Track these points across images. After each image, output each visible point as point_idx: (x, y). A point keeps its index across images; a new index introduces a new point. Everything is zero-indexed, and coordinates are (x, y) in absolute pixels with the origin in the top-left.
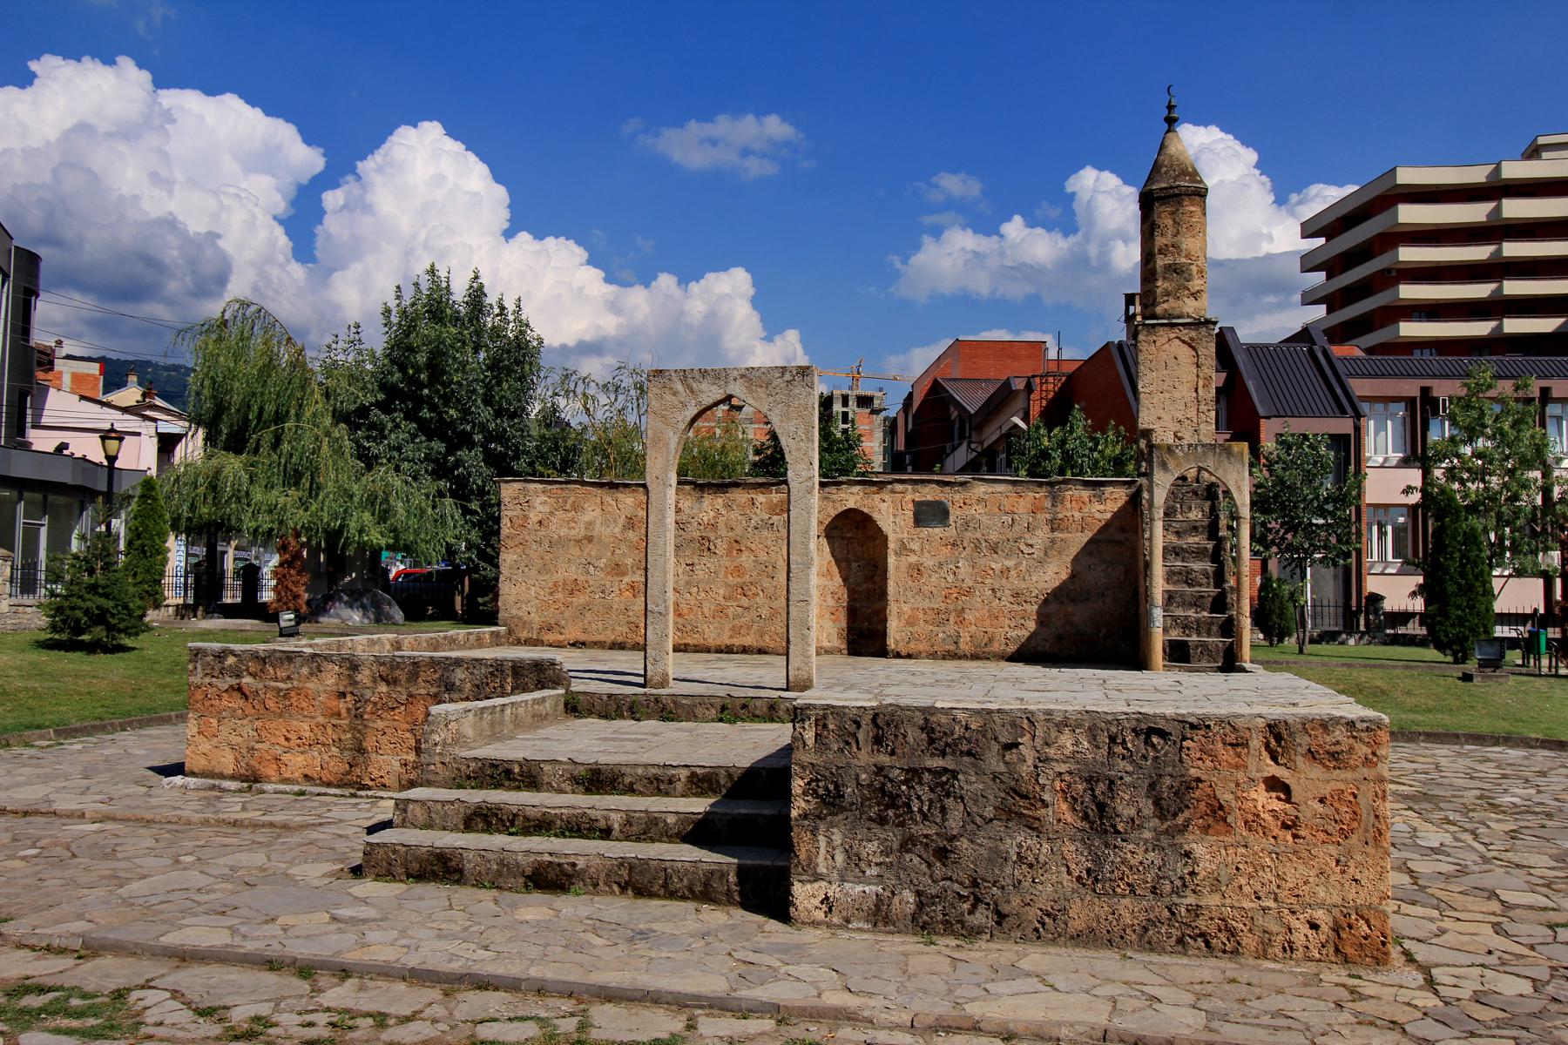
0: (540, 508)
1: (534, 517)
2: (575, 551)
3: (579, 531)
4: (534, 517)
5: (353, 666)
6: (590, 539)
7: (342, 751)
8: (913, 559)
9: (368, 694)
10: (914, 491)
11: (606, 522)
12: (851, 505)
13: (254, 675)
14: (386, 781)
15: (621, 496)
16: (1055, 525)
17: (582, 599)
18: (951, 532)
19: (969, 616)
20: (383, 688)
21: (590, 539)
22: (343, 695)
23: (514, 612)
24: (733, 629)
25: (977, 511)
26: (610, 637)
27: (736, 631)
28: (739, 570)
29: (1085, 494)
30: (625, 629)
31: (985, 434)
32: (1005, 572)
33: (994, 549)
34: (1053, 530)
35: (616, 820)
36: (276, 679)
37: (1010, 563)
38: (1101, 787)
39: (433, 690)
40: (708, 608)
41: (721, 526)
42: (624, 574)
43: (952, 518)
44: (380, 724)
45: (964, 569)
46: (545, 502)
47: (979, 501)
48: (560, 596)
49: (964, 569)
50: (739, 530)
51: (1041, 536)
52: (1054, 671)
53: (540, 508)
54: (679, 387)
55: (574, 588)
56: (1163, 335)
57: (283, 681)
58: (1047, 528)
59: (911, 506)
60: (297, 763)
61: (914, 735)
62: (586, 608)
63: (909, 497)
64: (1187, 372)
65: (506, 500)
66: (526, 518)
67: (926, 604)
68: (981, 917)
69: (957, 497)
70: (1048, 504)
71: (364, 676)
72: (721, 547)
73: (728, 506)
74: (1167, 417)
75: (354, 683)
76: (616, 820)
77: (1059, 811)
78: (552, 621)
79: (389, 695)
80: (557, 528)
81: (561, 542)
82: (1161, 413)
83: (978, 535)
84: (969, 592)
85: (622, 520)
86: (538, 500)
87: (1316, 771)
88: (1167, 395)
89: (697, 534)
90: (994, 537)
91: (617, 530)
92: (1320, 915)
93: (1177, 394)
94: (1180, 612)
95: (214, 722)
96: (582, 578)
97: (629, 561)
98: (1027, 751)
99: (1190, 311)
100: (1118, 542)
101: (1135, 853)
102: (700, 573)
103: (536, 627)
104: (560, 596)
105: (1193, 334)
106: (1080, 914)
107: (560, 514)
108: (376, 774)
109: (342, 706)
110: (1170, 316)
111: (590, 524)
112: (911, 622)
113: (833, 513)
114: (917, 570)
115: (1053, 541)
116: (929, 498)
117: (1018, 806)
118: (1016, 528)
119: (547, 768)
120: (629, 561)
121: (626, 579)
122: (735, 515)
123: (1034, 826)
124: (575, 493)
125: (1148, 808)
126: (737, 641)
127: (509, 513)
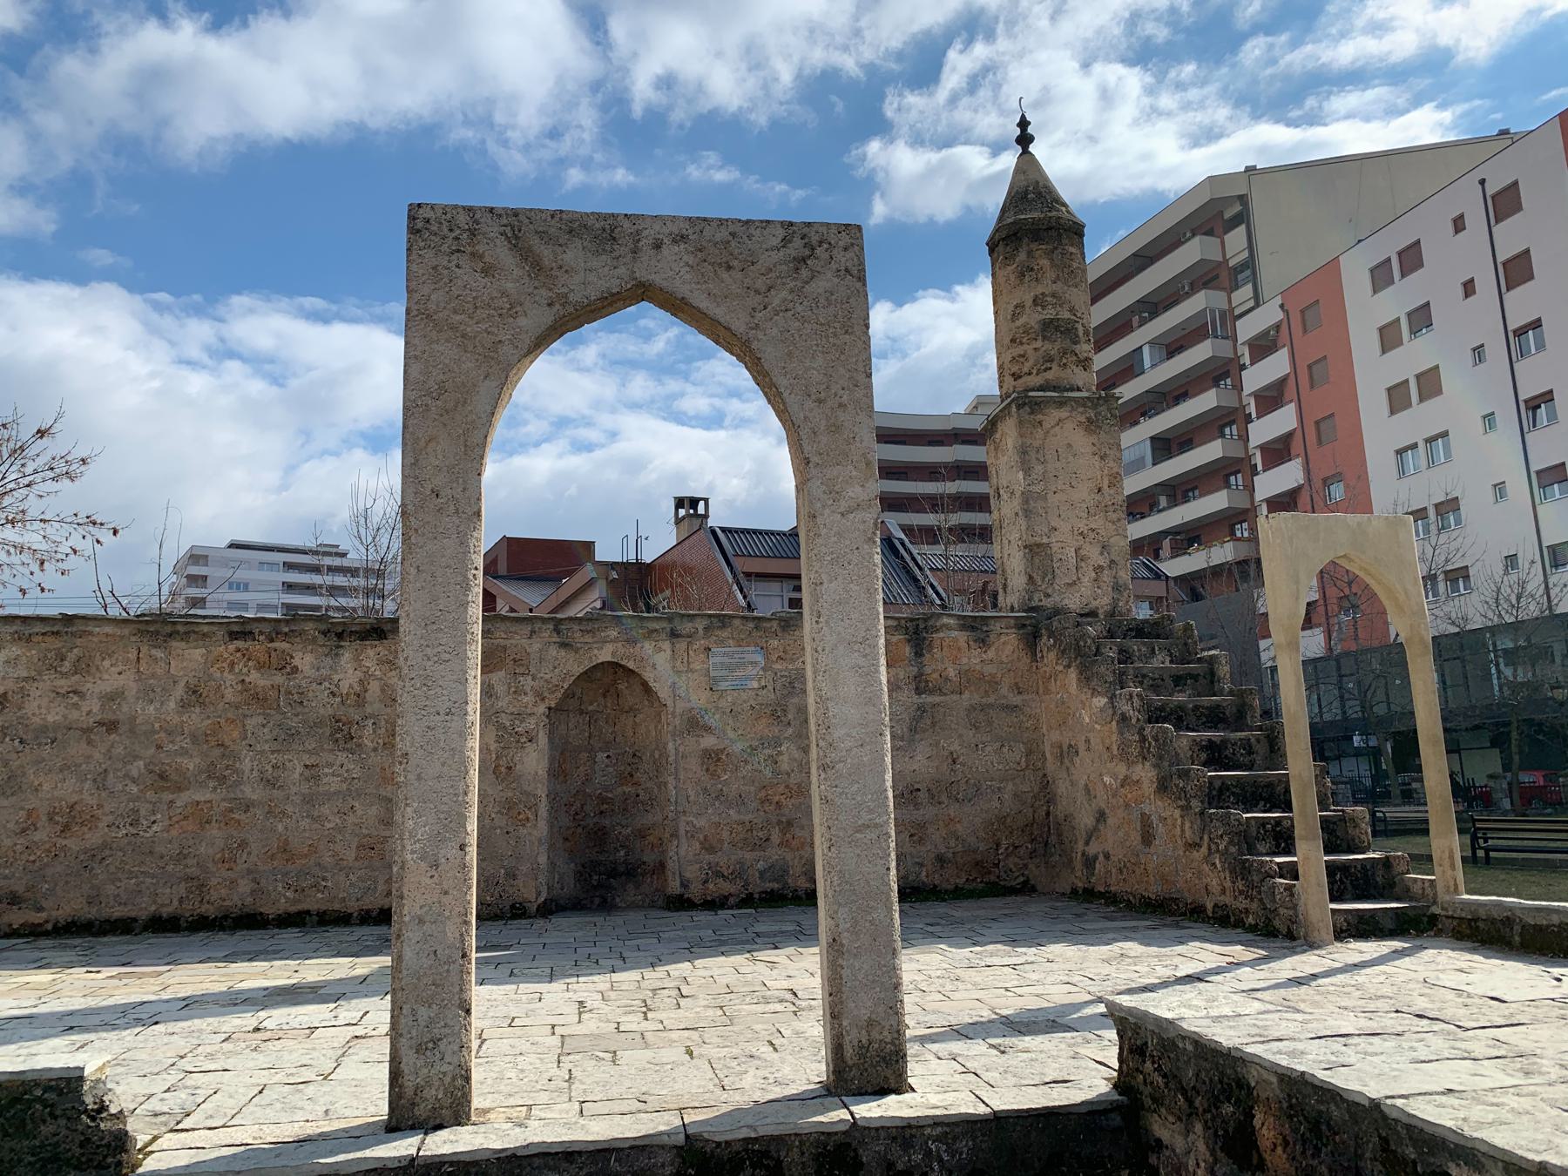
8: (709, 741)
11: (147, 694)
12: (605, 655)
21: (111, 726)
26: (144, 908)
34: (918, 691)
52: (1520, 965)
54: (502, 254)
70: (907, 650)
74: (1065, 528)
97: (191, 764)
112: (709, 848)
114: (712, 758)
121: (183, 798)
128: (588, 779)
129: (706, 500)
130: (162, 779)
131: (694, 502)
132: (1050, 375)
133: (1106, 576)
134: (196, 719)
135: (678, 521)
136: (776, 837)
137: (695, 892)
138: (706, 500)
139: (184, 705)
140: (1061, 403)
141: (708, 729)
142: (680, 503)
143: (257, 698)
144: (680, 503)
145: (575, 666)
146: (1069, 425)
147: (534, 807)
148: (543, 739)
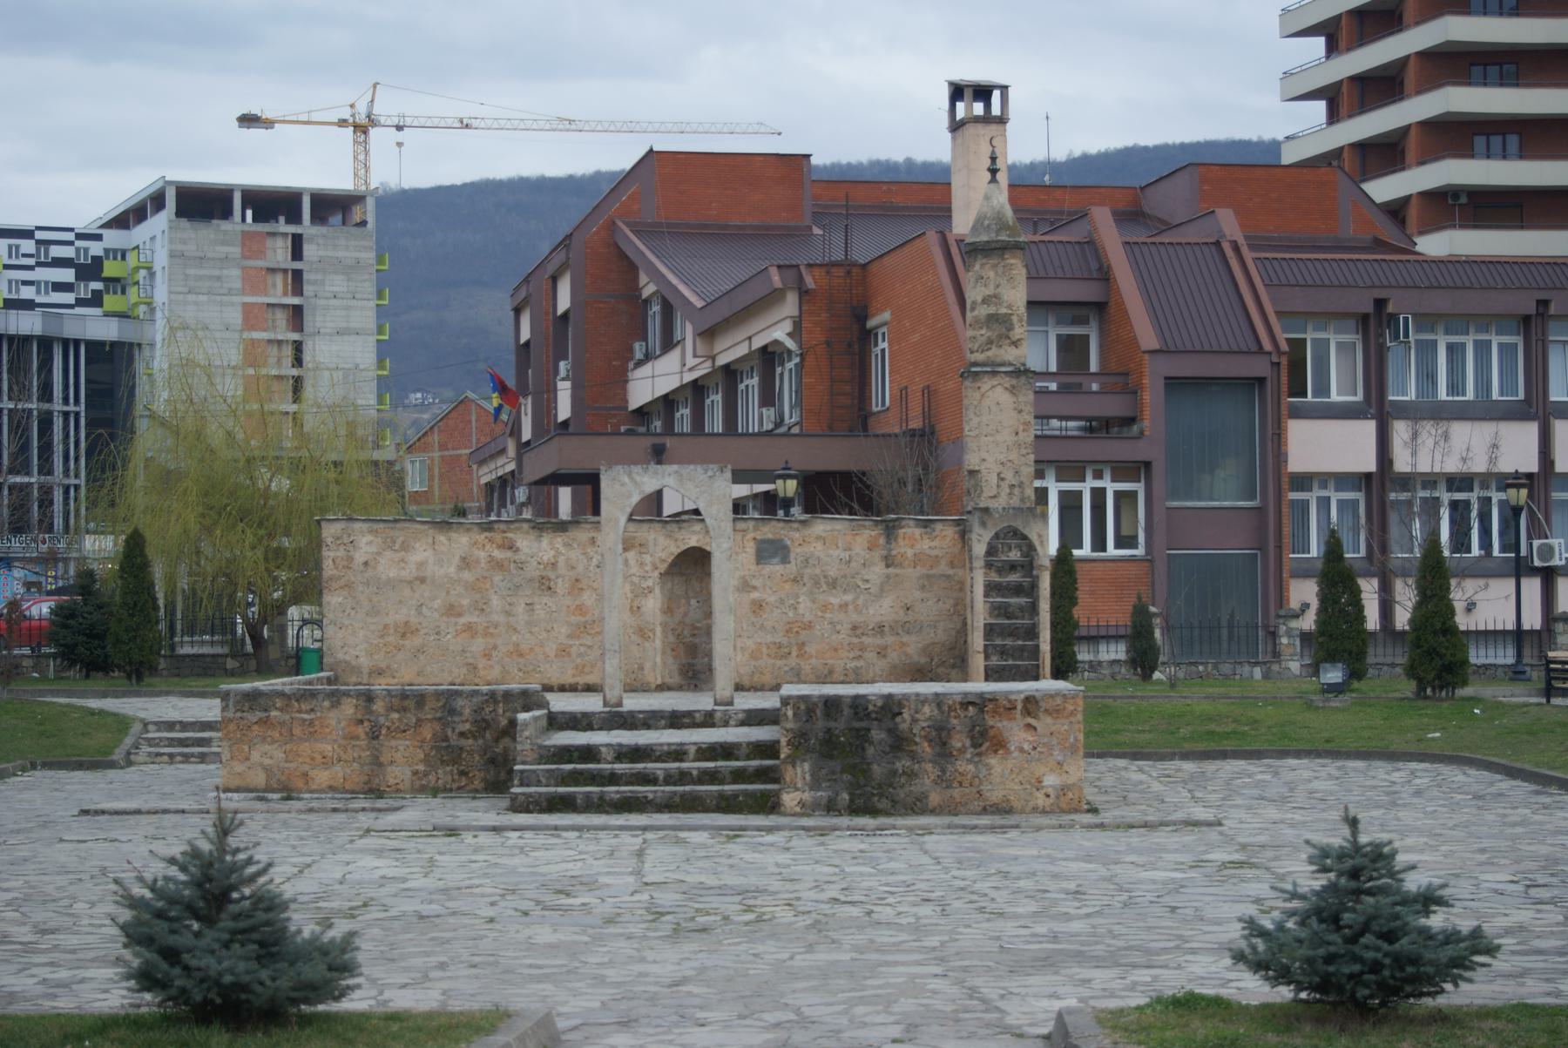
0: (366, 548)
1: (360, 557)
2: (407, 592)
3: (409, 572)
4: (360, 557)
5: (369, 697)
6: (423, 580)
7: (362, 765)
8: (755, 595)
9: (382, 720)
10: (756, 529)
12: (693, 542)
13: (281, 710)
14: (401, 786)
15: (454, 535)
16: (889, 561)
17: (416, 641)
18: (791, 568)
19: (811, 649)
20: (395, 716)
21: (423, 580)
22: (361, 722)
23: (340, 656)
24: (576, 668)
25: (817, 549)
27: (580, 669)
28: (581, 610)
29: (918, 532)
30: (464, 671)
31: (718, 347)
32: (844, 607)
33: (833, 584)
34: (888, 566)
35: (661, 774)
36: (300, 711)
37: (848, 598)
38: (944, 734)
39: (439, 715)
40: (551, 648)
41: (561, 564)
42: (460, 615)
43: (792, 556)
44: (393, 743)
45: (804, 603)
46: (371, 542)
47: (818, 538)
48: (391, 639)
49: (804, 603)
50: (580, 568)
51: (877, 571)
53: (366, 548)
55: (406, 631)
56: (986, 384)
57: (307, 712)
58: (883, 564)
59: (752, 544)
60: (322, 777)
61: (846, 711)
62: (420, 650)
63: (750, 535)
64: (1009, 419)
65: (329, 540)
66: (351, 559)
67: (769, 639)
68: (884, 804)
69: (797, 535)
70: (882, 541)
71: (379, 706)
72: (561, 586)
73: (567, 545)
74: (991, 459)
75: (371, 712)
76: (661, 774)
77: (925, 748)
78: (383, 666)
79: (400, 720)
80: (387, 568)
81: (392, 584)
82: (984, 455)
83: (818, 571)
84: (809, 626)
85: (456, 560)
86: (364, 540)
87: (1049, 720)
88: (990, 439)
89: (536, 574)
90: (832, 573)
91: (452, 569)
92: (1050, 791)
93: (999, 438)
94: (999, 642)
95: (246, 748)
96: (414, 620)
97: (465, 602)
98: (906, 716)
99: (1011, 358)
100: (948, 577)
101: (963, 766)
102: (540, 613)
103: (366, 671)
104: (391, 639)
105: (1014, 382)
106: (934, 798)
107: (388, 554)
108: (392, 782)
109: (360, 730)
110: (993, 364)
111: (421, 564)
113: (677, 551)
115: (888, 577)
116: (770, 536)
117: (899, 744)
118: (853, 564)
119: (603, 749)
120: (465, 602)
121: (462, 620)
122: (575, 554)
123: (913, 756)
124: (400, 534)
125: (968, 743)
126: (582, 680)
127: (332, 554)
128: (685, 615)
129: (1004, 89)
130: (452, 610)
131: (982, 92)
132: (990, 353)
133: (1016, 491)
134: (467, 576)
135: (956, 126)
136: (794, 653)
137: (746, 683)
138: (1004, 89)
139: (460, 569)
140: (994, 373)
141: (754, 588)
142: (957, 92)
143: (499, 566)
144: (957, 92)
145: (675, 549)
146: (999, 389)
147: (653, 630)
148: (657, 591)
